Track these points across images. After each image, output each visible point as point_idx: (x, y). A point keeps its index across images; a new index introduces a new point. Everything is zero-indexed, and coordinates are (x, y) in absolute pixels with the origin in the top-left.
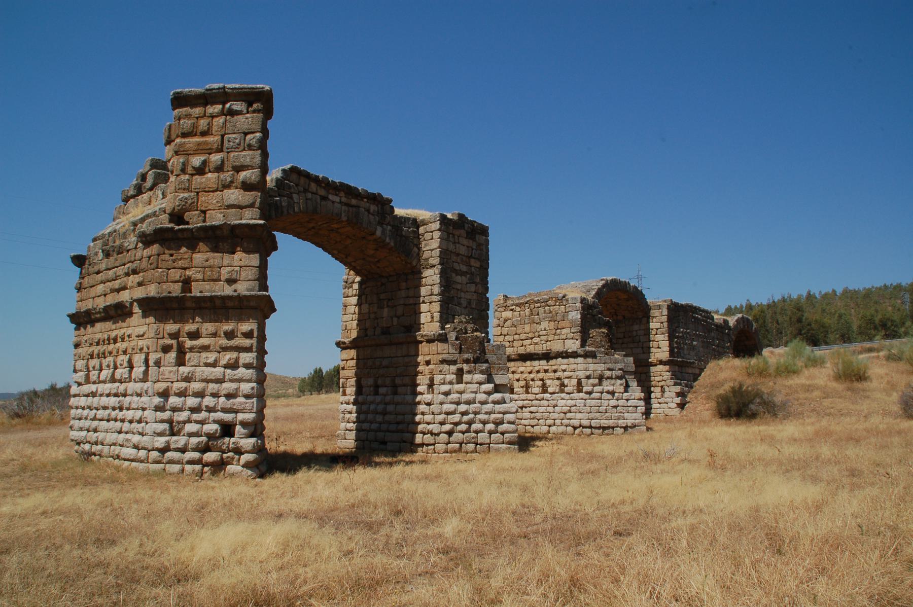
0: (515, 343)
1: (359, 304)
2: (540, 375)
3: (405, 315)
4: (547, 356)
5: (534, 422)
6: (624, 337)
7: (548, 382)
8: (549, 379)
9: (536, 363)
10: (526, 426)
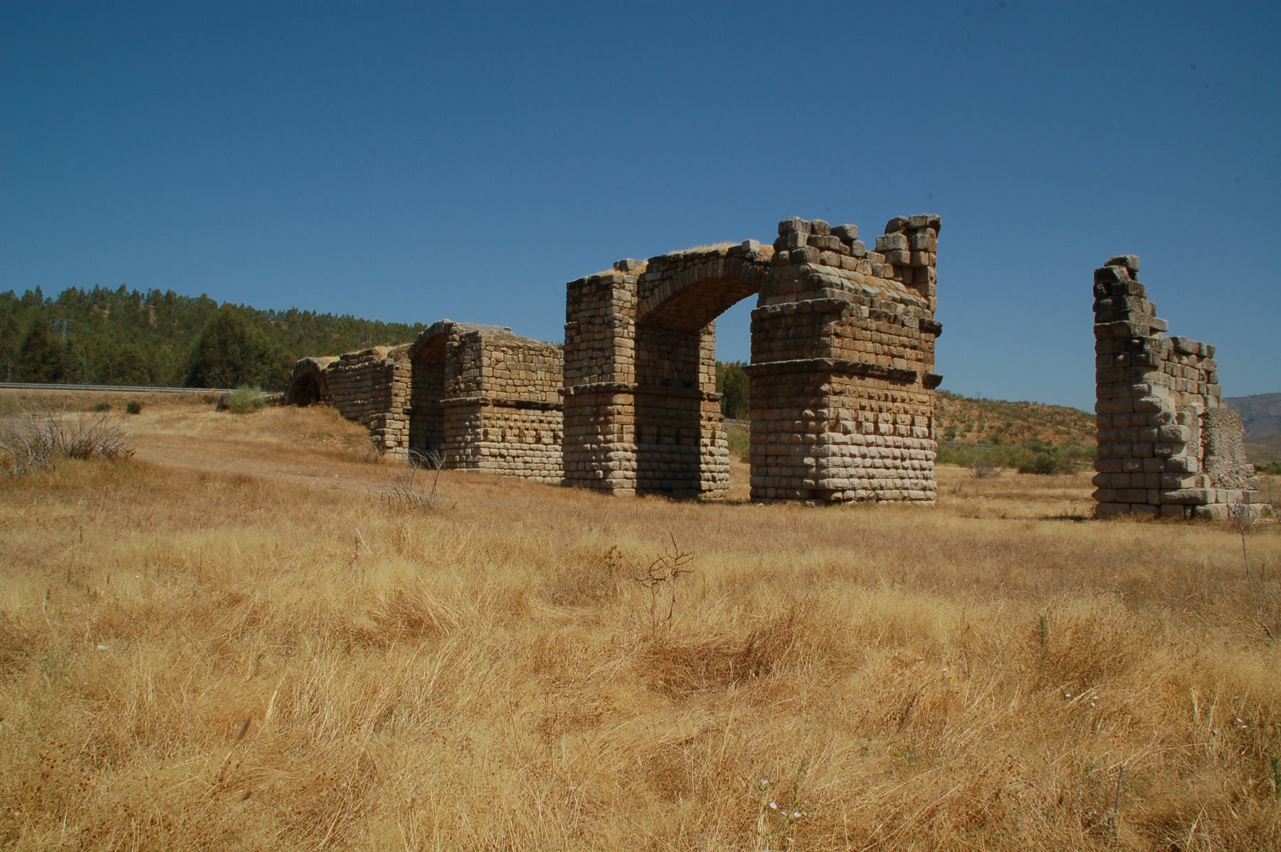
0: (508, 388)
1: (636, 349)
2: (536, 425)
4: (520, 405)
5: (528, 472)
6: (436, 384)
7: (543, 433)
8: (543, 430)
9: (531, 412)
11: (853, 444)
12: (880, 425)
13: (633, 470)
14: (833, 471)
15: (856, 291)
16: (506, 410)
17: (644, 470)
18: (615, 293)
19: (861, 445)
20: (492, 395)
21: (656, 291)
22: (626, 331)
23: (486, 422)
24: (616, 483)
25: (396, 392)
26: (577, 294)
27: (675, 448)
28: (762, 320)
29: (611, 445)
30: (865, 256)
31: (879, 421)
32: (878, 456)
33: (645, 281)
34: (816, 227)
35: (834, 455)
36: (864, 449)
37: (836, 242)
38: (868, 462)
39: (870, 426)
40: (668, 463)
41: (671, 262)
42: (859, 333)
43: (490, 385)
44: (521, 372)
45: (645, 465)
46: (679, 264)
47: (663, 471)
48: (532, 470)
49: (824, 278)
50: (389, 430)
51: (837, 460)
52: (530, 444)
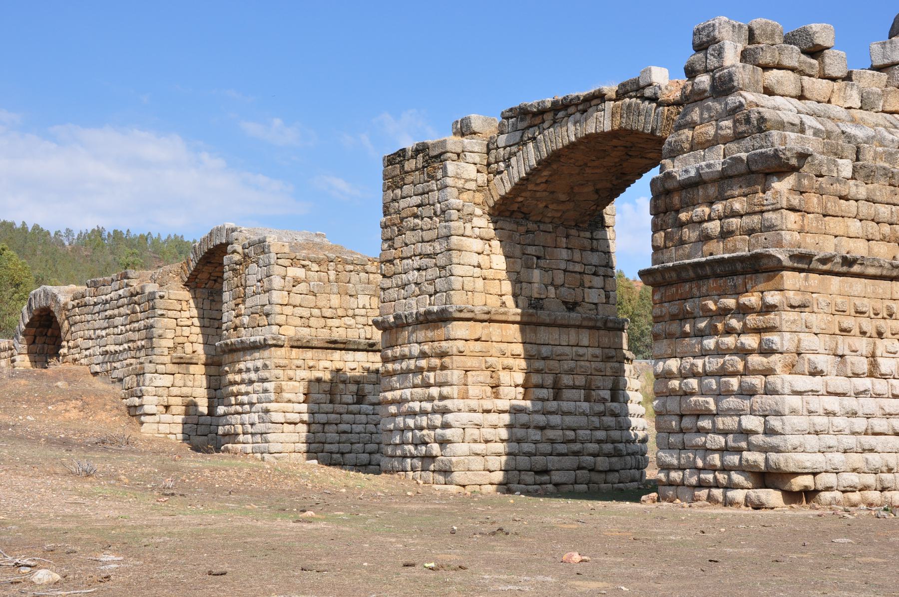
0: (313, 322)
3: (566, 285)
5: (346, 447)
10: (331, 453)
11: (830, 394)
12: (880, 360)
13: (503, 441)
14: (793, 440)
15: (829, 134)
16: (309, 354)
17: (519, 441)
18: (451, 167)
19: (844, 395)
20: (289, 331)
21: (513, 160)
22: (468, 225)
23: (279, 372)
24: (458, 463)
25: (160, 332)
26: (398, 172)
27: (553, 405)
28: (668, 192)
29: (448, 403)
30: (848, 78)
31: (878, 353)
32: (879, 413)
33: (498, 148)
34: (757, 32)
35: (794, 412)
36: (851, 403)
37: (793, 56)
38: (860, 424)
39: (863, 365)
40: (542, 428)
41: (535, 115)
42: (834, 205)
43: (284, 317)
44: (333, 297)
45: (520, 433)
46: (545, 116)
47: (536, 442)
48: (352, 443)
49: (767, 114)
50: (149, 389)
51: (801, 422)
52: (348, 404)
